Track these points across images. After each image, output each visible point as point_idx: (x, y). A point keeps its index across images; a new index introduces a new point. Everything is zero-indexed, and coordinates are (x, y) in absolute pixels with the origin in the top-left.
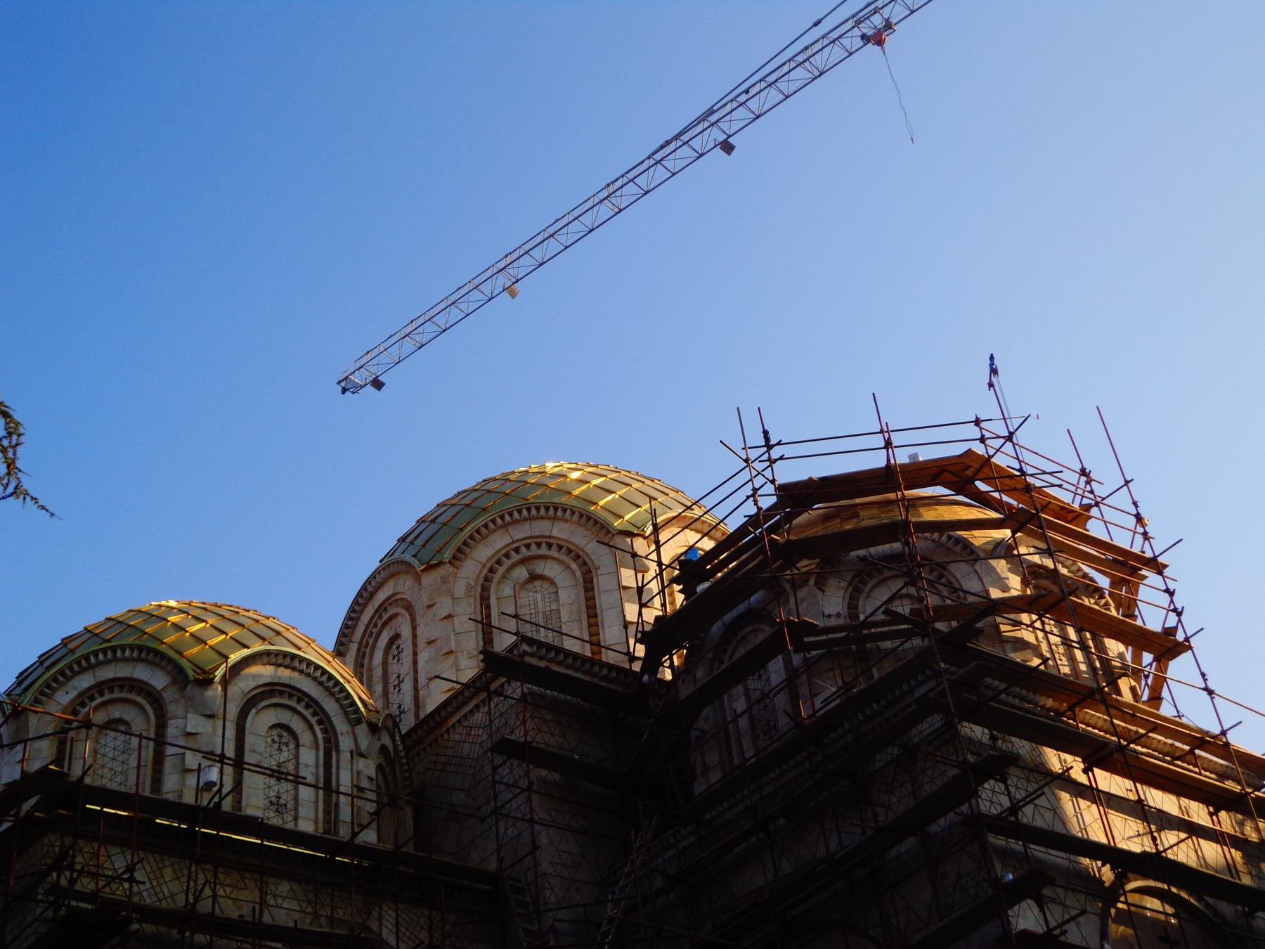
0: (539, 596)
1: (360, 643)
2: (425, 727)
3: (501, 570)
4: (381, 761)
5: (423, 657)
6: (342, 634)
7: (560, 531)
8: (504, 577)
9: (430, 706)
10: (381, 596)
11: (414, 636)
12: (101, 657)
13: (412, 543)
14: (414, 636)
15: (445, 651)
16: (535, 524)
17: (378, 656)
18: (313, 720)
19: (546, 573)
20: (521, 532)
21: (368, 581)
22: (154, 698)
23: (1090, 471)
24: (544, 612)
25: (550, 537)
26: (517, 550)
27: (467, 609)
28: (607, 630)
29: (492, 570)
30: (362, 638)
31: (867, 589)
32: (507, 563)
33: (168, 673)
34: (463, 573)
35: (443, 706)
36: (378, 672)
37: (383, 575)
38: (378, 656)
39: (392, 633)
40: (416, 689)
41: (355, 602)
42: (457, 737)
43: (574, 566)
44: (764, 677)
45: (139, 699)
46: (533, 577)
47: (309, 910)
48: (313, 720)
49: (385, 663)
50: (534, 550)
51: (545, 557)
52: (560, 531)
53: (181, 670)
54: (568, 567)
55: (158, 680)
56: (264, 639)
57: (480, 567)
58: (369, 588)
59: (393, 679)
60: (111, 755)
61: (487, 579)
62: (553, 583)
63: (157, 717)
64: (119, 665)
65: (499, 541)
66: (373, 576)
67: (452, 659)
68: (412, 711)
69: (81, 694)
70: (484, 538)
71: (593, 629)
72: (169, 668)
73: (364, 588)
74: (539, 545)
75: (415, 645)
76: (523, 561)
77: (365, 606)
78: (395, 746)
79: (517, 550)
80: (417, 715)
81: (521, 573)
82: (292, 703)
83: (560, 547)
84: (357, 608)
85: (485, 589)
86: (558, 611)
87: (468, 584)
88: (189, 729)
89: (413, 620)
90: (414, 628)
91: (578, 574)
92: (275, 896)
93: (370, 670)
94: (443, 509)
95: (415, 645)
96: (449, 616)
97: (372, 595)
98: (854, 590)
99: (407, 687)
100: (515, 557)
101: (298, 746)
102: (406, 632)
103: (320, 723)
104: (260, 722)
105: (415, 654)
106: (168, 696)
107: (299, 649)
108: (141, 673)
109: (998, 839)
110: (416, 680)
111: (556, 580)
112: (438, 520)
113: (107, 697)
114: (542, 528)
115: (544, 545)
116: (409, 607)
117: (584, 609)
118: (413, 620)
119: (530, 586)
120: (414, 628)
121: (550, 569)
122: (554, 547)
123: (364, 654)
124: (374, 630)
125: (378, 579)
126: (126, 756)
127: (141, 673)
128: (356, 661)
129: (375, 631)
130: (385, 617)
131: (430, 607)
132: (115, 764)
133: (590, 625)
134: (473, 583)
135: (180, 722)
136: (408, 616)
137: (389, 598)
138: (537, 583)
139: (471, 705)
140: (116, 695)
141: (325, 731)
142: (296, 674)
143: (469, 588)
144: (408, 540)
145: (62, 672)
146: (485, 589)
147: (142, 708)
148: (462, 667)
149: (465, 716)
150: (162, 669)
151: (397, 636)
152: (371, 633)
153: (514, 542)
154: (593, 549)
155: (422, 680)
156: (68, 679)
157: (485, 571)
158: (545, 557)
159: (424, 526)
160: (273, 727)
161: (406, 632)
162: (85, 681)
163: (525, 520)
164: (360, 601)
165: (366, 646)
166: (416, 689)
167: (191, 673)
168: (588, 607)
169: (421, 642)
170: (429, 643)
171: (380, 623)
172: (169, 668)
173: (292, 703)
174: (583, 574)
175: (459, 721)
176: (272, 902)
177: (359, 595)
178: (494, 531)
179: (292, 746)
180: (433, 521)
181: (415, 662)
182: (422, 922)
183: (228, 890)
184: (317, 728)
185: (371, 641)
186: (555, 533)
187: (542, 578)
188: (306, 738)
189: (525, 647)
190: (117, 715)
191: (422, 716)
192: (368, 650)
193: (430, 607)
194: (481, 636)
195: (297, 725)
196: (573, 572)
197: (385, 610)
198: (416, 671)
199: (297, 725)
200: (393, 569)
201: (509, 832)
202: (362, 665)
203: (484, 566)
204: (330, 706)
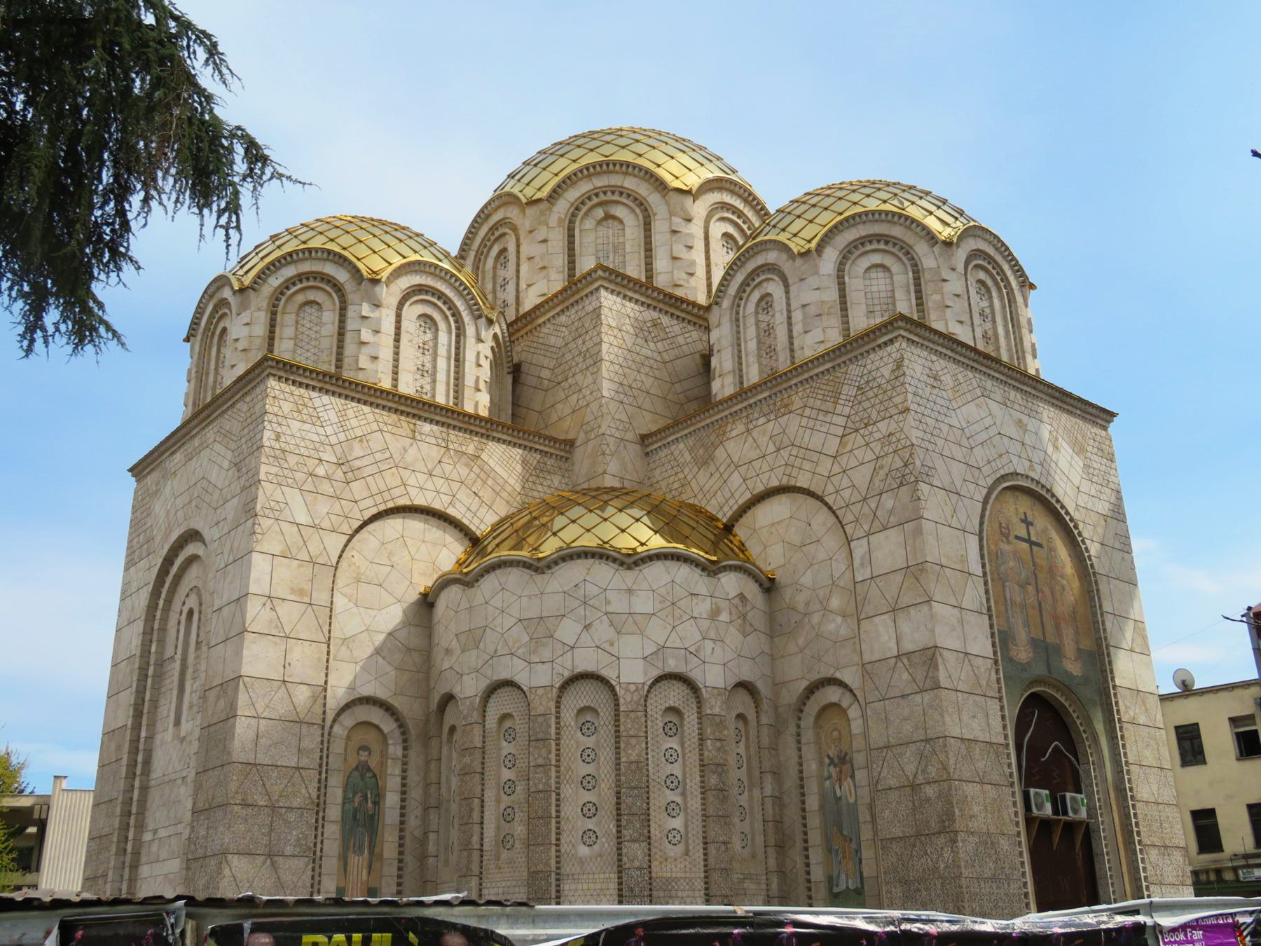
0: (611, 232)
1: (477, 252)
2: (524, 321)
3: (585, 209)
4: (493, 344)
5: (524, 268)
6: (464, 243)
7: (630, 183)
8: (586, 214)
9: (527, 305)
10: (495, 218)
11: (518, 252)
12: (301, 255)
13: (519, 180)
14: (518, 252)
15: (541, 266)
16: (612, 176)
17: (490, 262)
18: (448, 313)
20: (600, 182)
21: (485, 206)
22: (338, 288)
23: (1037, 370)
24: (613, 244)
25: (622, 187)
26: (597, 195)
27: (557, 239)
28: (658, 262)
29: (577, 209)
30: (479, 248)
31: (853, 257)
32: (590, 204)
33: (349, 272)
34: (555, 209)
35: (537, 307)
36: (489, 275)
37: (496, 203)
38: (490, 262)
39: (502, 247)
40: (518, 291)
41: (475, 221)
42: (546, 330)
43: (638, 211)
44: (771, 313)
45: (328, 288)
46: (608, 217)
47: (444, 445)
48: (448, 313)
49: (495, 268)
50: (609, 197)
51: (617, 202)
52: (630, 183)
53: (358, 271)
54: (634, 211)
55: (342, 276)
56: (416, 252)
57: (569, 205)
58: (486, 212)
59: (500, 281)
60: (308, 326)
61: (573, 215)
62: (621, 222)
63: (340, 302)
64: (314, 262)
66: (489, 203)
67: (545, 272)
68: (514, 306)
69: (287, 281)
70: (574, 183)
71: (648, 260)
72: (350, 268)
73: (482, 211)
74: (613, 193)
75: (518, 258)
76: (600, 204)
77: (481, 224)
78: (503, 333)
79: (597, 195)
80: (517, 310)
81: (600, 213)
82: (434, 300)
83: (629, 196)
84: (476, 225)
85: (571, 222)
86: (624, 243)
87: (560, 218)
88: (364, 314)
89: (518, 240)
90: (518, 246)
91: (641, 217)
92: (421, 434)
93: (483, 272)
94: (543, 156)
95: (518, 258)
96: (545, 241)
97: (488, 216)
98: (843, 258)
99: (511, 288)
100: (595, 200)
101: (437, 330)
102: (512, 248)
103: (453, 315)
105: (518, 265)
107: (440, 261)
108: (329, 269)
109: (1070, 926)
110: (518, 284)
111: (625, 221)
112: (540, 165)
113: (305, 284)
114: (615, 180)
115: (617, 193)
116: (515, 229)
117: (643, 244)
118: (518, 240)
119: (605, 223)
120: (518, 246)
121: (619, 211)
122: (624, 195)
123: (480, 260)
124: (488, 244)
125: (493, 205)
126: (318, 328)
127: (329, 269)
128: (473, 264)
129: (488, 244)
130: (497, 234)
131: (531, 232)
132: (311, 332)
133: (646, 257)
134: (563, 217)
135: (357, 307)
136: (513, 237)
137: (501, 220)
138: (610, 221)
139: (558, 309)
140: (311, 283)
141: (456, 322)
143: (560, 221)
144: (517, 178)
145: (272, 263)
146: (571, 222)
147: (330, 295)
148: (552, 278)
149: (553, 317)
150: (345, 268)
151: (504, 250)
152: (486, 245)
153: (595, 189)
154: (654, 199)
155: (523, 286)
156: (278, 269)
157: (572, 209)
158: (617, 202)
159: (528, 168)
160: (420, 316)
161: (512, 248)
162: (290, 271)
163: (605, 172)
164: (479, 220)
165: (482, 254)
166: (518, 291)
167: (365, 273)
168: (646, 244)
169: (523, 257)
170: (530, 259)
171: (492, 238)
172: (350, 268)
173: (434, 300)
174: (644, 218)
175: (549, 320)
176: (419, 438)
177: (478, 216)
178: (581, 179)
179: (433, 330)
180: (535, 165)
181: (518, 271)
182: (518, 458)
183: (390, 427)
185: (485, 250)
186: (626, 185)
187: (614, 218)
188: (442, 325)
189: (600, 273)
190: (312, 298)
191: (521, 312)
192: (483, 257)
193: (531, 232)
194: (566, 257)
195: (437, 316)
196: (637, 216)
197: (497, 229)
198: (518, 277)
199: (437, 316)
200: (504, 199)
201: (580, 402)
202: (478, 268)
203: (572, 205)
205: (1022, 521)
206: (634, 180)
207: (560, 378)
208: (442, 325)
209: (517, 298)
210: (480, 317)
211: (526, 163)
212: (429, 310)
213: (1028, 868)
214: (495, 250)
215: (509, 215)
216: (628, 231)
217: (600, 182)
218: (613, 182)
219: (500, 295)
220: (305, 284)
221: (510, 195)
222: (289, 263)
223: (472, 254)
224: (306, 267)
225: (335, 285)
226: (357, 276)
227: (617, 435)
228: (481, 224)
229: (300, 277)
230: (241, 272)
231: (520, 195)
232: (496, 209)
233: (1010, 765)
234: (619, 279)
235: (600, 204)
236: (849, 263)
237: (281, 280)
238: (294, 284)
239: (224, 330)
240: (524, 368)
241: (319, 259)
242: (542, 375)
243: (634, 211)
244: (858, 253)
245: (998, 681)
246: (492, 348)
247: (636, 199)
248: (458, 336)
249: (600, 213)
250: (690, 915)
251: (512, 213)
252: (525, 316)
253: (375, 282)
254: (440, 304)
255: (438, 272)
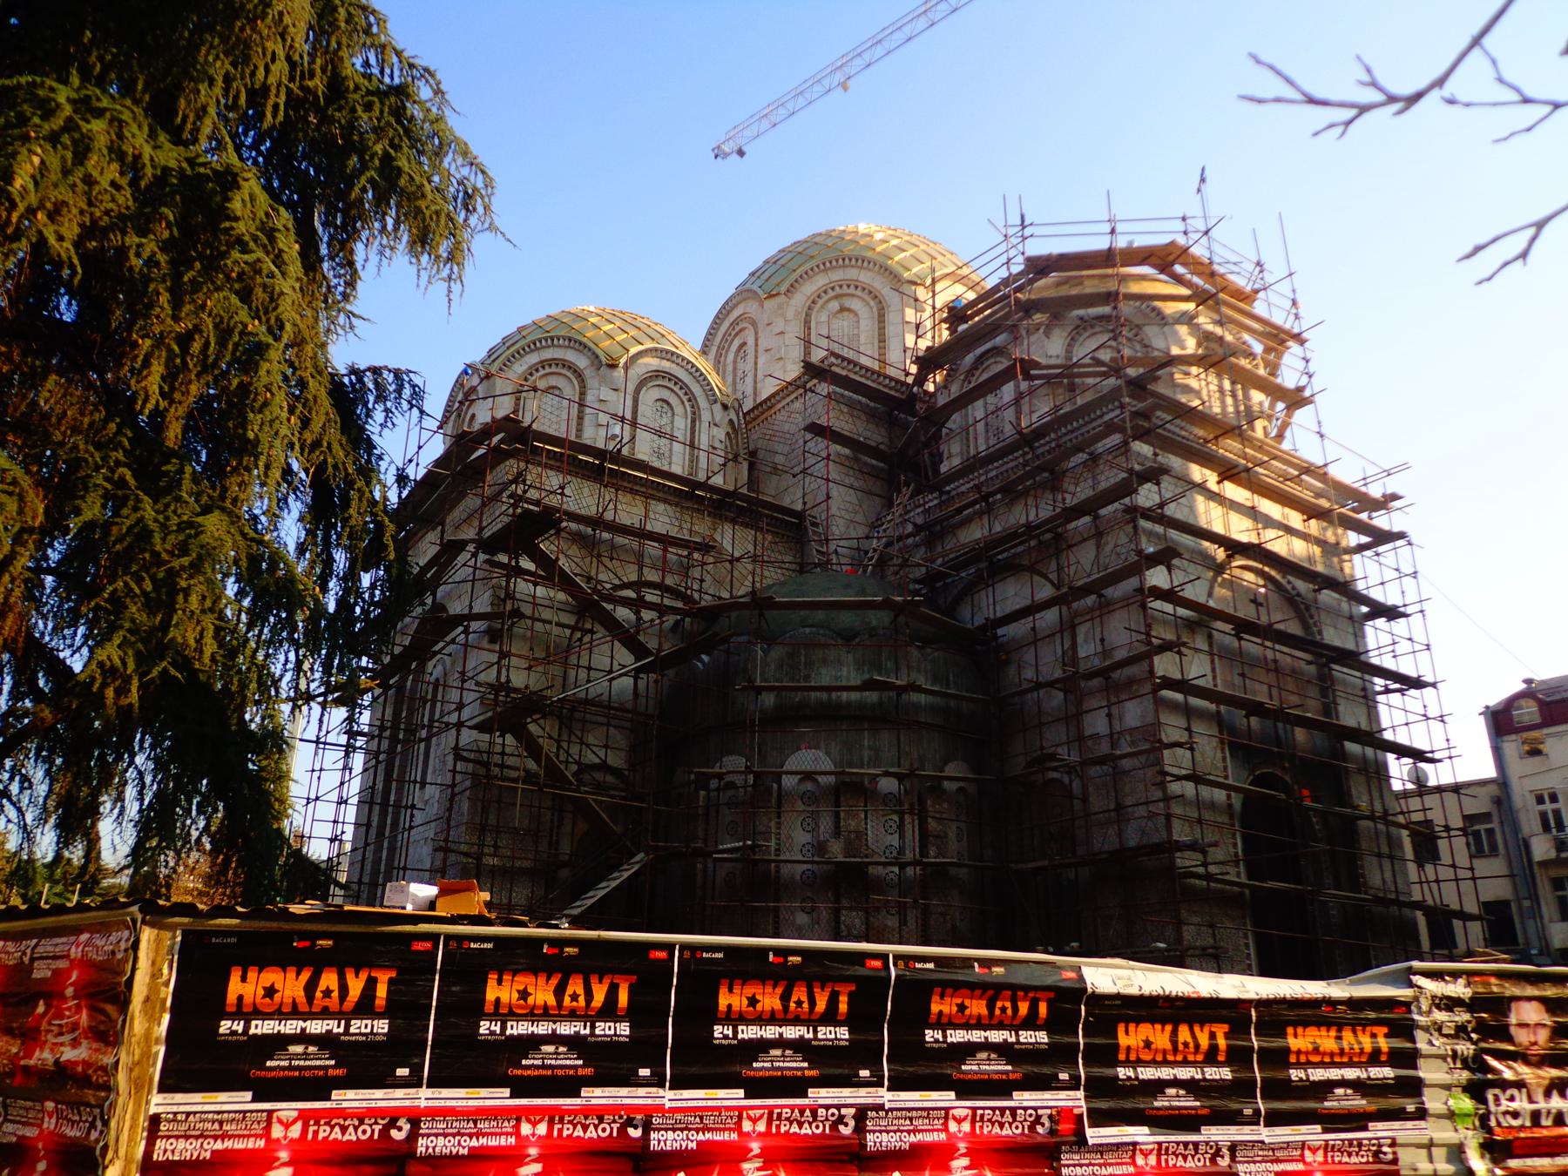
0: (845, 323)
3: (821, 302)
6: (707, 339)
7: (865, 277)
9: (764, 396)
11: (757, 345)
14: (757, 345)
17: (731, 356)
19: (852, 307)
20: (836, 276)
21: (727, 303)
22: (579, 374)
31: (1082, 339)
32: (825, 297)
34: (793, 302)
35: (773, 395)
36: (730, 368)
38: (731, 356)
41: (717, 317)
45: (569, 374)
46: (843, 309)
49: (735, 362)
51: (853, 295)
52: (865, 277)
54: (868, 304)
55: (581, 362)
59: (740, 373)
62: (856, 314)
65: (820, 281)
66: (730, 299)
67: (781, 362)
69: (530, 368)
70: (810, 278)
73: (723, 307)
75: (756, 351)
76: (836, 297)
80: (755, 400)
81: (835, 305)
83: (864, 289)
85: (808, 315)
89: (756, 333)
91: (875, 309)
93: (725, 366)
95: (756, 351)
97: (729, 313)
99: (749, 380)
100: (831, 294)
102: (751, 342)
104: (649, 396)
106: (588, 373)
108: (570, 356)
111: (860, 313)
113: (548, 370)
114: (852, 274)
116: (754, 324)
118: (756, 333)
119: (840, 316)
120: (757, 339)
121: (855, 304)
127: (570, 356)
130: (737, 329)
138: (846, 314)
142: (674, 366)
143: (797, 313)
146: (808, 315)
158: (853, 295)
161: (751, 342)
162: (533, 359)
169: (760, 349)
177: (720, 312)
179: (669, 414)
181: (756, 363)
184: (687, 404)
187: (849, 310)
188: (679, 409)
195: (673, 400)
196: (871, 308)
198: (756, 369)
199: (673, 400)
204: (696, 389)
205: (1252, 601)
206: (869, 274)
207: (793, 463)
208: (679, 409)
209: (755, 388)
210: (715, 402)
211: (766, 262)
212: (666, 394)
213: (1252, 951)
214: (736, 343)
215: (748, 310)
216: (863, 323)
217: (836, 276)
218: (848, 276)
219: (739, 387)
220: (548, 370)
221: (749, 291)
222: (532, 351)
223: (714, 349)
224: (548, 354)
225: (575, 371)
226: (596, 362)
227: (847, 516)
228: (723, 320)
229: (543, 364)
230: (489, 361)
231: (758, 290)
232: (736, 306)
233: (1235, 845)
234: (851, 366)
235: (836, 297)
236: (1077, 344)
237: (525, 367)
238: (537, 370)
239: (473, 416)
240: (761, 454)
241: (560, 346)
242: (777, 461)
243: (868, 304)
244: (1087, 334)
245: (1224, 759)
246: (728, 434)
247: (870, 292)
248: (693, 421)
249: (835, 305)
250: (1545, 687)
251: (751, 308)
252: (761, 404)
253: (613, 366)
254: (676, 389)
255: (674, 358)
